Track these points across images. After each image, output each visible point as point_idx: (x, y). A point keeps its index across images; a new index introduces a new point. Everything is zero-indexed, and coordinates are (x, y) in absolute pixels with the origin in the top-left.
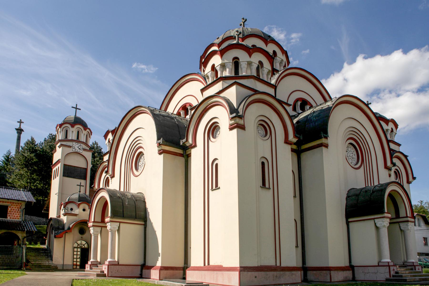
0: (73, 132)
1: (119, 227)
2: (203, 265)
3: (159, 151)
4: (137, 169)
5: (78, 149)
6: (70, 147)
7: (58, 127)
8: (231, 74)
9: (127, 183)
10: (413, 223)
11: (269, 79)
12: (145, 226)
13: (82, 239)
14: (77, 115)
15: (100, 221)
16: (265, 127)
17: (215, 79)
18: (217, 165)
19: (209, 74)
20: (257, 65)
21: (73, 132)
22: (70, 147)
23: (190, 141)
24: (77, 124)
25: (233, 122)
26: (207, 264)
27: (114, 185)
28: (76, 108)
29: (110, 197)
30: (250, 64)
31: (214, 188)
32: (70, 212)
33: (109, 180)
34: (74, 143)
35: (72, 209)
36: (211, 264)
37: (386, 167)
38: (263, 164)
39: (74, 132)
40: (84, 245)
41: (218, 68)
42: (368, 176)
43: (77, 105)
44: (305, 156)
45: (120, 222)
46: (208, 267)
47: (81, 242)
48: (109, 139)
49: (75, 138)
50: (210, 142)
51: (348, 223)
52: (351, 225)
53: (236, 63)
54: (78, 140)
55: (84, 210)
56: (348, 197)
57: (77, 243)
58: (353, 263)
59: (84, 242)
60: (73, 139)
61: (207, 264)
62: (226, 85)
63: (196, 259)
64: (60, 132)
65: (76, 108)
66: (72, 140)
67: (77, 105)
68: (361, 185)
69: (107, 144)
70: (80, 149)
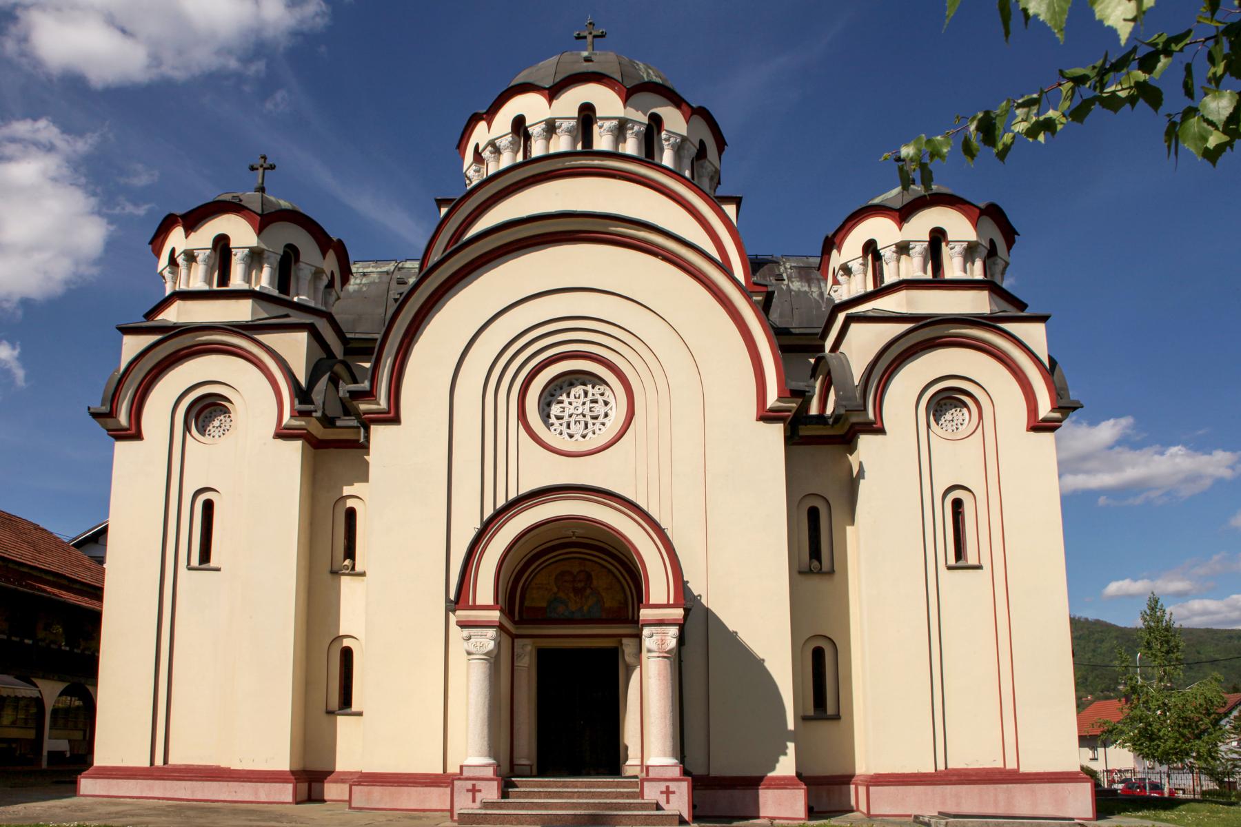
2: (148, 765)
31: (195, 561)
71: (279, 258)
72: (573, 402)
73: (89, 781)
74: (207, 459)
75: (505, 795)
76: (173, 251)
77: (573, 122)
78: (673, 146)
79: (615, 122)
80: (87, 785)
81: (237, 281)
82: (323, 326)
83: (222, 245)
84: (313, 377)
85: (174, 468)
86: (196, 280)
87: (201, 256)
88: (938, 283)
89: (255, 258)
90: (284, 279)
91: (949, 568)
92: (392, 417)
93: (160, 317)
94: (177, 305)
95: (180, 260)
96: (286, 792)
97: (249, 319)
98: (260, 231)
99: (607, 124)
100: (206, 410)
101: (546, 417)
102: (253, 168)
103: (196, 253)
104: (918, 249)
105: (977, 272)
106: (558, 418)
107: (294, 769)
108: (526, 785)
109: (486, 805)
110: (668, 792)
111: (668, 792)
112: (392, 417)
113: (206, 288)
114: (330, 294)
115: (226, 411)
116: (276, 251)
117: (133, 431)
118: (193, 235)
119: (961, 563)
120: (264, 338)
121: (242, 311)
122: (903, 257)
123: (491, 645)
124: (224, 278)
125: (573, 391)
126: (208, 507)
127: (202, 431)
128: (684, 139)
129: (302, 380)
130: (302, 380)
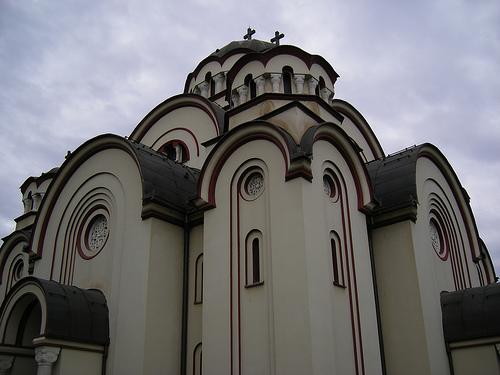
3: (143, 213)
9: (67, 267)
10: (101, 355)
12: (105, 358)
15: (13, 343)
16: (331, 180)
17: (249, 99)
18: (256, 242)
19: (240, 90)
23: (204, 196)
25: (295, 166)
27: (42, 271)
29: (48, 295)
30: (308, 78)
31: (251, 282)
33: (22, 265)
37: (476, 261)
38: (333, 241)
41: (257, 81)
42: (458, 273)
44: (380, 234)
48: (30, 193)
51: (449, 354)
52: (455, 354)
53: (287, 73)
56: (444, 305)
68: (451, 289)
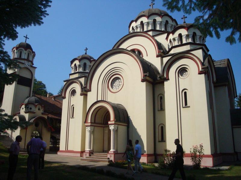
0: (25, 53)
1: (118, 128)
2: (65, 150)
4: (112, 87)
5: (28, 65)
6: (23, 63)
7: (15, 49)
8: (201, 42)
11: (202, 41)
13: (36, 130)
14: (27, 42)
20: (165, 23)
21: (25, 53)
22: (23, 63)
24: (28, 49)
26: (67, 150)
28: (26, 38)
31: (184, 106)
32: (30, 110)
34: (26, 61)
35: (31, 109)
36: (68, 149)
39: (26, 54)
40: (37, 134)
43: (27, 35)
45: (118, 125)
46: (67, 151)
47: (36, 132)
49: (26, 58)
50: (179, 78)
51: (232, 128)
52: (234, 129)
54: (28, 60)
55: (39, 109)
57: (38, 133)
58: (80, 150)
59: (37, 132)
60: (25, 58)
61: (67, 150)
62: (192, 48)
63: (62, 147)
64: (16, 53)
65: (26, 38)
66: (24, 59)
67: (27, 35)
69: (73, 67)
70: (29, 65)
71: (192, 35)
72: (117, 83)
73: (60, 153)
74: (185, 82)
75: (90, 156)
76: (170, 39)
77: (152, 23)
78: (159, 24)
79: (147, 23)
80: (59, 153)
81: (184, 42)
82: (204, 47)
83: (180, 36)
84: (204, 59)
85: (69, 102)
86: (176, 43)
87: (176, 39)
88: (182, 45)
89: (187, 36)
90: (194, 39)
91: (183, 108)
92: (90, 91)
93: (170, 53)
94: (173, 49)
95: (172, 41)
96: (79, 155)
97: (189, 49)
98: (187, 30)
99: (145, 24)
100: (182, 71)
101: (112, 87)
102: (182, 18)
103: (175, 38)
104: (191, 36)
105: (190, 40)
106: (115, 86)
107: (82, 151)
108: (95, 154)
109: (86, 157)
110: (111, 156)
111: (111, 156)
112: (90, 91)
113: (178, 44)
114: (204, 41)
115: (187, 71)
116: (191, 33)
117: (167, 78)
118: (174, 35)
119: (186, 106)
120: (192, 52)
121: (187, 48)
122: (175, 42)
123: (90, 129)
124: (182, 42)
125: (117, 81)
126: (185, 93)
127: (182, 75)
128: (161, 22)
129: (202, 61)
130: (202, 61)
